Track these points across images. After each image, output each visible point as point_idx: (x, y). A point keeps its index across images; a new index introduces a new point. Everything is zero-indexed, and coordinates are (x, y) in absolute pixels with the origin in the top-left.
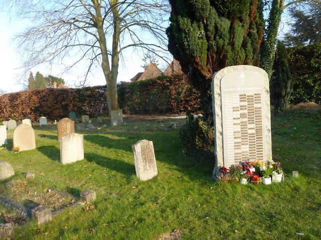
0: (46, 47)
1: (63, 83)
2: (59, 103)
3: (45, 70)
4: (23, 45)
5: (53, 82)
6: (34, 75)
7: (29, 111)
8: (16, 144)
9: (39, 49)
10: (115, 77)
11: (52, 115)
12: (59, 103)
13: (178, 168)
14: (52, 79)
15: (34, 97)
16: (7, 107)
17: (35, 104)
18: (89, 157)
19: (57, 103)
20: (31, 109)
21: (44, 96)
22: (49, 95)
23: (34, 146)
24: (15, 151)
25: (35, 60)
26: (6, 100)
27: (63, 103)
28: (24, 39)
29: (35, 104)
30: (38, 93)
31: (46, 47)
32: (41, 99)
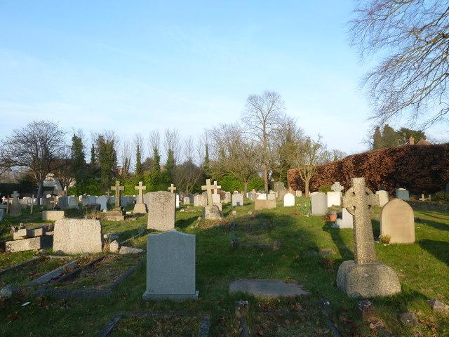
0: (410, 83)
1: (424, 137)
2: (426, 168)
3: (399, 122)
4: (378, 88)
5: (408, 137)
6: (381, 130)
7: (378, 178)
8: (385, 231)
9: (398, 89)
10: (97, 254)
11: (414, 186)
12: (426, 168)
13: (162, 168)
14: (406, 133)
15: (387, 160)
16: (350, 173)
17: (388, 169)
18: (424, 243)
19: (422, 168)
20: (382, 176)
21: (402, 158)
22: (410, 155)
23: (412, 239)
24: (383, 242)
25: (393, 106)
26: (350, 164)
27: (433, 168)
28: (381, 76)
29: (388, 169)
30: (393, 152)
31: (410, 83)
32: (398, 161)
